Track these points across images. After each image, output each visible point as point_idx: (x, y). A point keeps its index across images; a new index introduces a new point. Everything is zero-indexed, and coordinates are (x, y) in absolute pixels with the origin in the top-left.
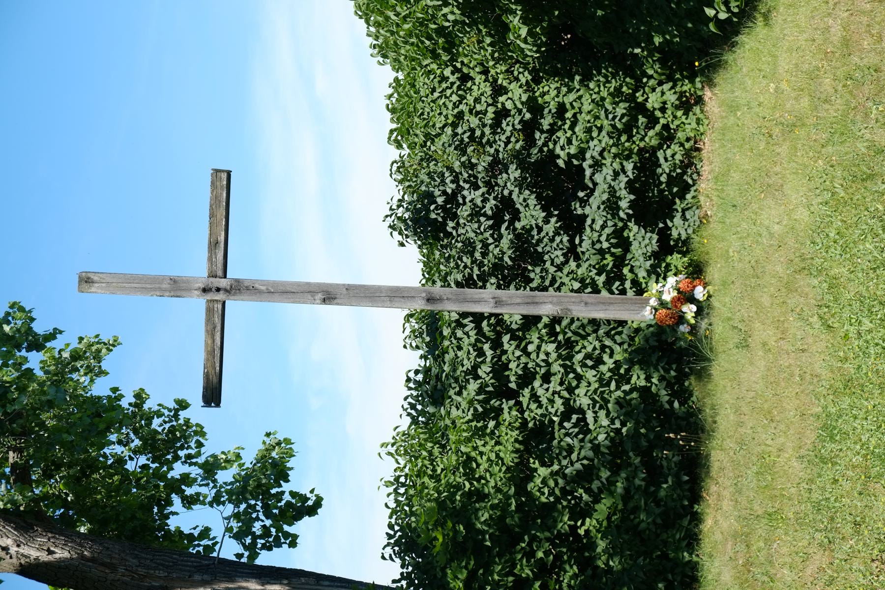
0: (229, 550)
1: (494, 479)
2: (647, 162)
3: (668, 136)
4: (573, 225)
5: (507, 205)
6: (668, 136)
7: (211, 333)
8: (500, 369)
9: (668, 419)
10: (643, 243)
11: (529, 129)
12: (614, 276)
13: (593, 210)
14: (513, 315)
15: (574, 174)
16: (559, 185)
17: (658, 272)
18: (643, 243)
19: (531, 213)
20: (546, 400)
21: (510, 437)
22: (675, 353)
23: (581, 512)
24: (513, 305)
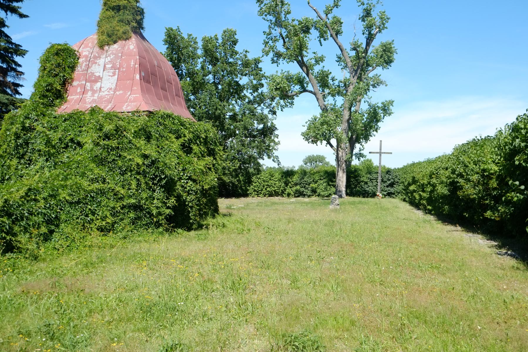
0: (354, 152)
1: (362, 179)
2: (394, 194)
3: (396, 196)
4: (387, 187)
5: (390, 180)
6: (396, 196)
7: (340, 44)
8: (373, 179)
9: (368, 195)
10: (385, 193)
11: (398, 182)
12: (382, 191)
13: (389, 188)
14: (378, 181)
15: (393, 187)
16: (392, 185)
17: (382, 194)
18: (385, 193)
19: (389, 182)
20: (370, 184)
21: (366, 181)
22: (374, 195)
23: (359, 187)
24: (379, 180)
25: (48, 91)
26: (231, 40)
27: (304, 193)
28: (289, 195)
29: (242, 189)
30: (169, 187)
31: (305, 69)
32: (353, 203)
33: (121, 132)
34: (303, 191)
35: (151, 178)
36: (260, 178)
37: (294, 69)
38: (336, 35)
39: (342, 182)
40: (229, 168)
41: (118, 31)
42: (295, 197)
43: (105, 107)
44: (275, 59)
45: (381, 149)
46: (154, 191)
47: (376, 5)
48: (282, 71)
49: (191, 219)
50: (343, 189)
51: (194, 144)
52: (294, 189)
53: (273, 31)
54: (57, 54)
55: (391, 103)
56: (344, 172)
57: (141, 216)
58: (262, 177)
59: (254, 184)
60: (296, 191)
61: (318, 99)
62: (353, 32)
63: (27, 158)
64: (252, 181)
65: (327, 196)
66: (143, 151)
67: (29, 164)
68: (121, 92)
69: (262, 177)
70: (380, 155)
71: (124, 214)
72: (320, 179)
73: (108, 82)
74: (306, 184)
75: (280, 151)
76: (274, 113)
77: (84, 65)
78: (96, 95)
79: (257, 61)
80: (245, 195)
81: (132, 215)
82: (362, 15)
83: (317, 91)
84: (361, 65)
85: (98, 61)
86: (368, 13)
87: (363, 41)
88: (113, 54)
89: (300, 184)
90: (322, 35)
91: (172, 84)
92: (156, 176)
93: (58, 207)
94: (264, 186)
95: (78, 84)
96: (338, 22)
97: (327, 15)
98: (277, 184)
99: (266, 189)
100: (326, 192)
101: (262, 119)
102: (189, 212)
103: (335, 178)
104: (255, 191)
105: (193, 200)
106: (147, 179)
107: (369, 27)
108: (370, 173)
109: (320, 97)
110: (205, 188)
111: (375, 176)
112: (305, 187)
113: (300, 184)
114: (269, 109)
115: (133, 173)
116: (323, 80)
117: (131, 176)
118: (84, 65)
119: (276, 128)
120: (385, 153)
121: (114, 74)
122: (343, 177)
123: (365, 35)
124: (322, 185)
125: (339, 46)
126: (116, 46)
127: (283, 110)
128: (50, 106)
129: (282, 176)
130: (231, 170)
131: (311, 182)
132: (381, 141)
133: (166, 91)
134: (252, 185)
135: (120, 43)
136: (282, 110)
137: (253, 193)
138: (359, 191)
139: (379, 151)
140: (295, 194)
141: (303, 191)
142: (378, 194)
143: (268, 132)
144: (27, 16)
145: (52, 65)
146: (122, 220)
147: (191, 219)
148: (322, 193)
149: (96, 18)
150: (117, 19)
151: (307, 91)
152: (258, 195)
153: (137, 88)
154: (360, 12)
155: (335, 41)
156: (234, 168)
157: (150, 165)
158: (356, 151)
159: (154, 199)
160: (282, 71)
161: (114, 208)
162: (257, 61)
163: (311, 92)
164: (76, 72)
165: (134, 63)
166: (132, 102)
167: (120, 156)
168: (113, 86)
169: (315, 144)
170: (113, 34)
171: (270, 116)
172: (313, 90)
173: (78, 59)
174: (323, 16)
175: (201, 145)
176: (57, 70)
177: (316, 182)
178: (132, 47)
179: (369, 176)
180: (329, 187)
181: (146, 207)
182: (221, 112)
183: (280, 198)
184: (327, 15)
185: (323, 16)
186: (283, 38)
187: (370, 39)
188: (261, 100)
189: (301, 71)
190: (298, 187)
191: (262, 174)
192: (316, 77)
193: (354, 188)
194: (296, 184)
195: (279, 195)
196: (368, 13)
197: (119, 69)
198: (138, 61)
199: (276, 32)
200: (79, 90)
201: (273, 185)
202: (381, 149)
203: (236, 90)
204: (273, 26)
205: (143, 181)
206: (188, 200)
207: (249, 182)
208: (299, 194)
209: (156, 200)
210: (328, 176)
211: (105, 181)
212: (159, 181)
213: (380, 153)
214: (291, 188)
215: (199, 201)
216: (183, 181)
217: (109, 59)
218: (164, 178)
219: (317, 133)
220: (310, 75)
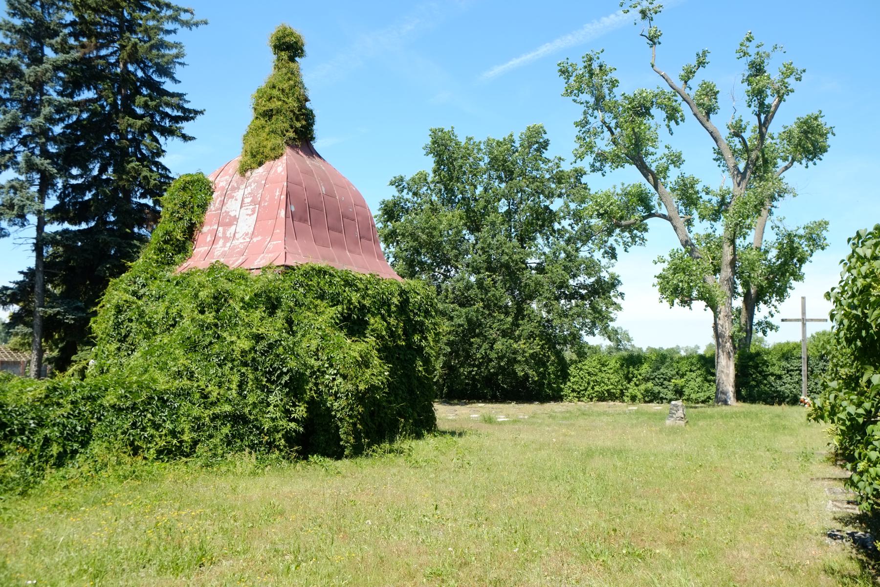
0: (755, 321)
7: (711, 129)
8: (792, 370)
20: (786, 379)
25: (165, 242)
26: (537, 142)
27: (661, 395)
28: (633, 398)
29: (552, 389)
30: (295, 386)
31: (650, 177)
32: (746, 415)
33: (225, 300)
34: (659, 393)
35: (266, 372)
36: (581, 369)
37: (629, 176)
38: (708, 114)
39: (728, 375)
40: (524, 352)
41: (265, 147)
42: (646, 402)
43: (233, 264)
44: (598, 164)
45: (804, 313)
46: (270, 392)
47: (772, 55)
48: (623, 184)
49: (342, 440)
50: (730, 389)
51: (374, 315)
52: (643, 387)
53: (591, 119)
54: (184, 189)
55: (823, 225)
56: (729, 357)
57: (241, 431)
58: (586, 367)
59: (572, 380)
60: (646, 391)
61: (675, 229)
62: (735, 107)
63: (129, 340)
64: (569, 375)
65: (703, 402)
66: (254, 330)
67: (133, 351)
68: (259, 238)
69: (586, 367)
70: (804, 325)
71: (215, 428)
72: (691, 371)
73: (246, 224)
74: (665, 379)
75: (620, 320)
76: (613, 256)
77: (218, 201)
78: (228, 245)
79: (579, 174)
80: (557, 397)
81: (226, 430)
82: (747, 74)
83: (673, 214)
84: (757, 165)
85: (235, 194)
86: (758, 69)
87: (751, 122)
88: (255, 182)
89: (654, 379)
90: (673, 115)
91: (354, 220)
92: (275, 370)
93: (93, 415)
94: (589, 384)
95: (209, 230)
96: (710, 92)
97: (686, 82)
98: (611, 379)
99: (593, 388)
100: (702, 394)
101: (591, 267)
102: (338, 428)
103: (714, 367)
104: (573, 391)
105: (343, 408)
106: (259, 373)
107: (759, 94)
108: (787, 359)
109: (680, 223)
110: (360, 388)
111: (795, 363)
112: (662, 384)
113: (654, 379)
114: (602, 251)
115: (236, 363)
116: (688, 195)
117: (232, 369)
118: (218, 201)
119: (619, 282)
120: (812, 320)
121: (253, 211)
122: (728, 367)
123: (753, 108)
124: (693, 382)
125: (711, 133)
126: (261, 170)
127: (629, 249)
128: (168, 264)
129: (622, 365)
130: (527, 355)
131: (673, 376)
132: (803, 298)
133: (341, 232)
134: (569, 380)
135: (267, 164)
136: (626, 251)
137: (571, 395)
138: (766, 393)
139: (800, 317)
140: (644, 398)
141: (659, 393)
142: (802, 397)
143: (603, 289)
144: (194, 138)
145: (175, 204)
146: (211, 436)
147: (342, 440)
148: (693, 396)
149: (244, 129)
150: (267, 130)
151: (654, 215)
152: (579, 398)
153: (280, 231)
154: (743, 68)
155: (703, 125)
156: (532, 351)
157: (267, 352)
158: (758, 317)
159: (268, 405)
160: (623, 184)
161: (198, 419)
162: (579, 174)
163: (664, 217)
164: (208, 213)
165: (279, 194)
166: (270, 252)
167: (218, 337)
168: (250, 230)
169: (687, 308)
170: (257, 153)
171: (604, 262)
172: (667, 214)
173: (212, 193)
174: (679, 85)
175: (390, 316)
176: (182, 211)
177: (682, 376)
178: (280, 169)
179: (784, 363)
180: (707, 384)
181: (252, 417)
182: (510, 258)
183: (617, 403)
184: (686, 82)
185: (679, 85)
186: (610, 129)
187: (765, 114)
188: (586, 235)
189: (644, 180)
190: (650, 385)
191: (586, 362)
192: (673, 190)
193: (756, 386)
194: (647, 380)
195: (617, 398)
196: (758, 69)
197: (259, 204)
198: (285, 189)
199: (597, 119)
200: (209, 239)
201: (606, 380)
202: (804, 313)
203: (543, 220)
204: (590, 111)
205: (251, 376)
206: (335, 408)
207: (564, 374)
208: (653, 397)
209: (272, 407)
210: (703, 365)
211: (192, 376)
212: (279, 377)
213: (804, 321)
214: (637, 385)
215: (352, 409)
216: (327, 377)
217: (249, 190)
218: (286, 374)
219: (678, 288)
220: (660, 186)
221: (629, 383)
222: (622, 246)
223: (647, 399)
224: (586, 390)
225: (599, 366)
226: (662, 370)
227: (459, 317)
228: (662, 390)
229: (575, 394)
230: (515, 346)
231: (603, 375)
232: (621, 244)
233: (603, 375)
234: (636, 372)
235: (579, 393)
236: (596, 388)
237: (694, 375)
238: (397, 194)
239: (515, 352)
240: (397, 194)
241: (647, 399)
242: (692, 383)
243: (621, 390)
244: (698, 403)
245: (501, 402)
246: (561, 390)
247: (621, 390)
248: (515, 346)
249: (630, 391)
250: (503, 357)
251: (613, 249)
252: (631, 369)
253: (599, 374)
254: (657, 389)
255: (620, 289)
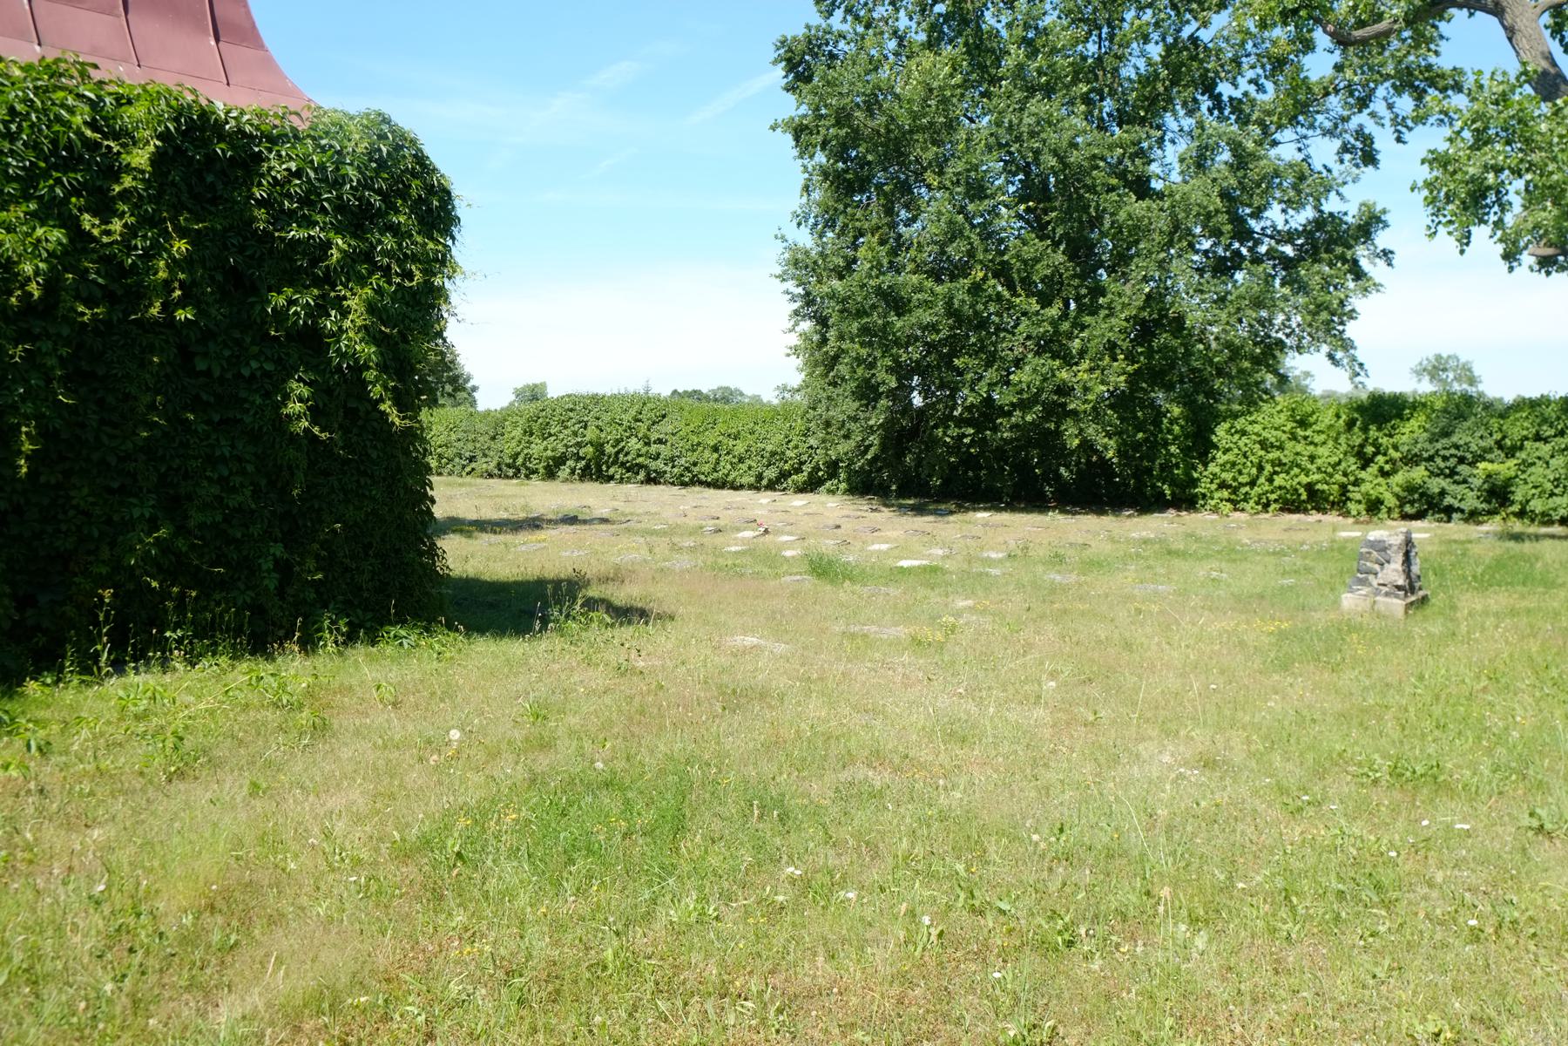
27: (1448, 500)
28: (1374, 506)
36: (1243, 433)
40: (1086, 389)
42: (1405, 517)
58: (1257, 428)
61: (1511, 33)
69: (1257, 428)
72: (1538, 438)
74: (1462, 460)
76: (1370, 158)
80: (1186, 500)
89: (1431, 459)
98: (1327, 455)
99: (1270, 480)
101: (1304, 183)
104: (1223, 485)
127: (1407, 136)
129: (1350, 424)
136: (1399, 140)
141: (1443, 493)
148: (1537, 505)
183: (1332, 518)
190: (1418, 474)
194: (1412, 460)
201: (1305, 462)
214: (1384, 474)
221: (1363, 468)
222: (1389, 131)
223: (1408, 509)
224: (1252, 483)
225: (1290, 425)
226: (1454, 439)
227: (927, 304)
228: (1451, 488)
229: (1225, 494)
230: (1064, 374)
231: (1299, 448)
232: (1387, 122)
233: (1299, 448)
234: (1384, 441)
235: (1235, 491)
236: (1278, 481)
237: (1545, 449)
238: (816, 19)
239: (1064, 390)
240: (816, 19)
241: (1408, 509)
242: (1538, 470)
243: (1343, 487)
244: (1550, 523)
245: (1011, 507)
246: (1194, 483)
247: (1343, 487)
248: (1064, 374)
249: (1365, 488)
250: (1035, 399)
251: (1367, 140)
252: (1373, 432)
253: (1289, 445)
254: (1435, 485)
255: (1382, 239)
